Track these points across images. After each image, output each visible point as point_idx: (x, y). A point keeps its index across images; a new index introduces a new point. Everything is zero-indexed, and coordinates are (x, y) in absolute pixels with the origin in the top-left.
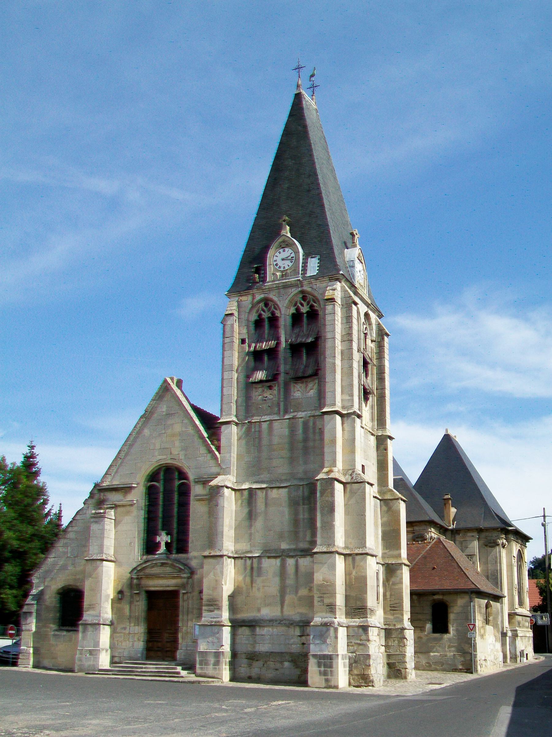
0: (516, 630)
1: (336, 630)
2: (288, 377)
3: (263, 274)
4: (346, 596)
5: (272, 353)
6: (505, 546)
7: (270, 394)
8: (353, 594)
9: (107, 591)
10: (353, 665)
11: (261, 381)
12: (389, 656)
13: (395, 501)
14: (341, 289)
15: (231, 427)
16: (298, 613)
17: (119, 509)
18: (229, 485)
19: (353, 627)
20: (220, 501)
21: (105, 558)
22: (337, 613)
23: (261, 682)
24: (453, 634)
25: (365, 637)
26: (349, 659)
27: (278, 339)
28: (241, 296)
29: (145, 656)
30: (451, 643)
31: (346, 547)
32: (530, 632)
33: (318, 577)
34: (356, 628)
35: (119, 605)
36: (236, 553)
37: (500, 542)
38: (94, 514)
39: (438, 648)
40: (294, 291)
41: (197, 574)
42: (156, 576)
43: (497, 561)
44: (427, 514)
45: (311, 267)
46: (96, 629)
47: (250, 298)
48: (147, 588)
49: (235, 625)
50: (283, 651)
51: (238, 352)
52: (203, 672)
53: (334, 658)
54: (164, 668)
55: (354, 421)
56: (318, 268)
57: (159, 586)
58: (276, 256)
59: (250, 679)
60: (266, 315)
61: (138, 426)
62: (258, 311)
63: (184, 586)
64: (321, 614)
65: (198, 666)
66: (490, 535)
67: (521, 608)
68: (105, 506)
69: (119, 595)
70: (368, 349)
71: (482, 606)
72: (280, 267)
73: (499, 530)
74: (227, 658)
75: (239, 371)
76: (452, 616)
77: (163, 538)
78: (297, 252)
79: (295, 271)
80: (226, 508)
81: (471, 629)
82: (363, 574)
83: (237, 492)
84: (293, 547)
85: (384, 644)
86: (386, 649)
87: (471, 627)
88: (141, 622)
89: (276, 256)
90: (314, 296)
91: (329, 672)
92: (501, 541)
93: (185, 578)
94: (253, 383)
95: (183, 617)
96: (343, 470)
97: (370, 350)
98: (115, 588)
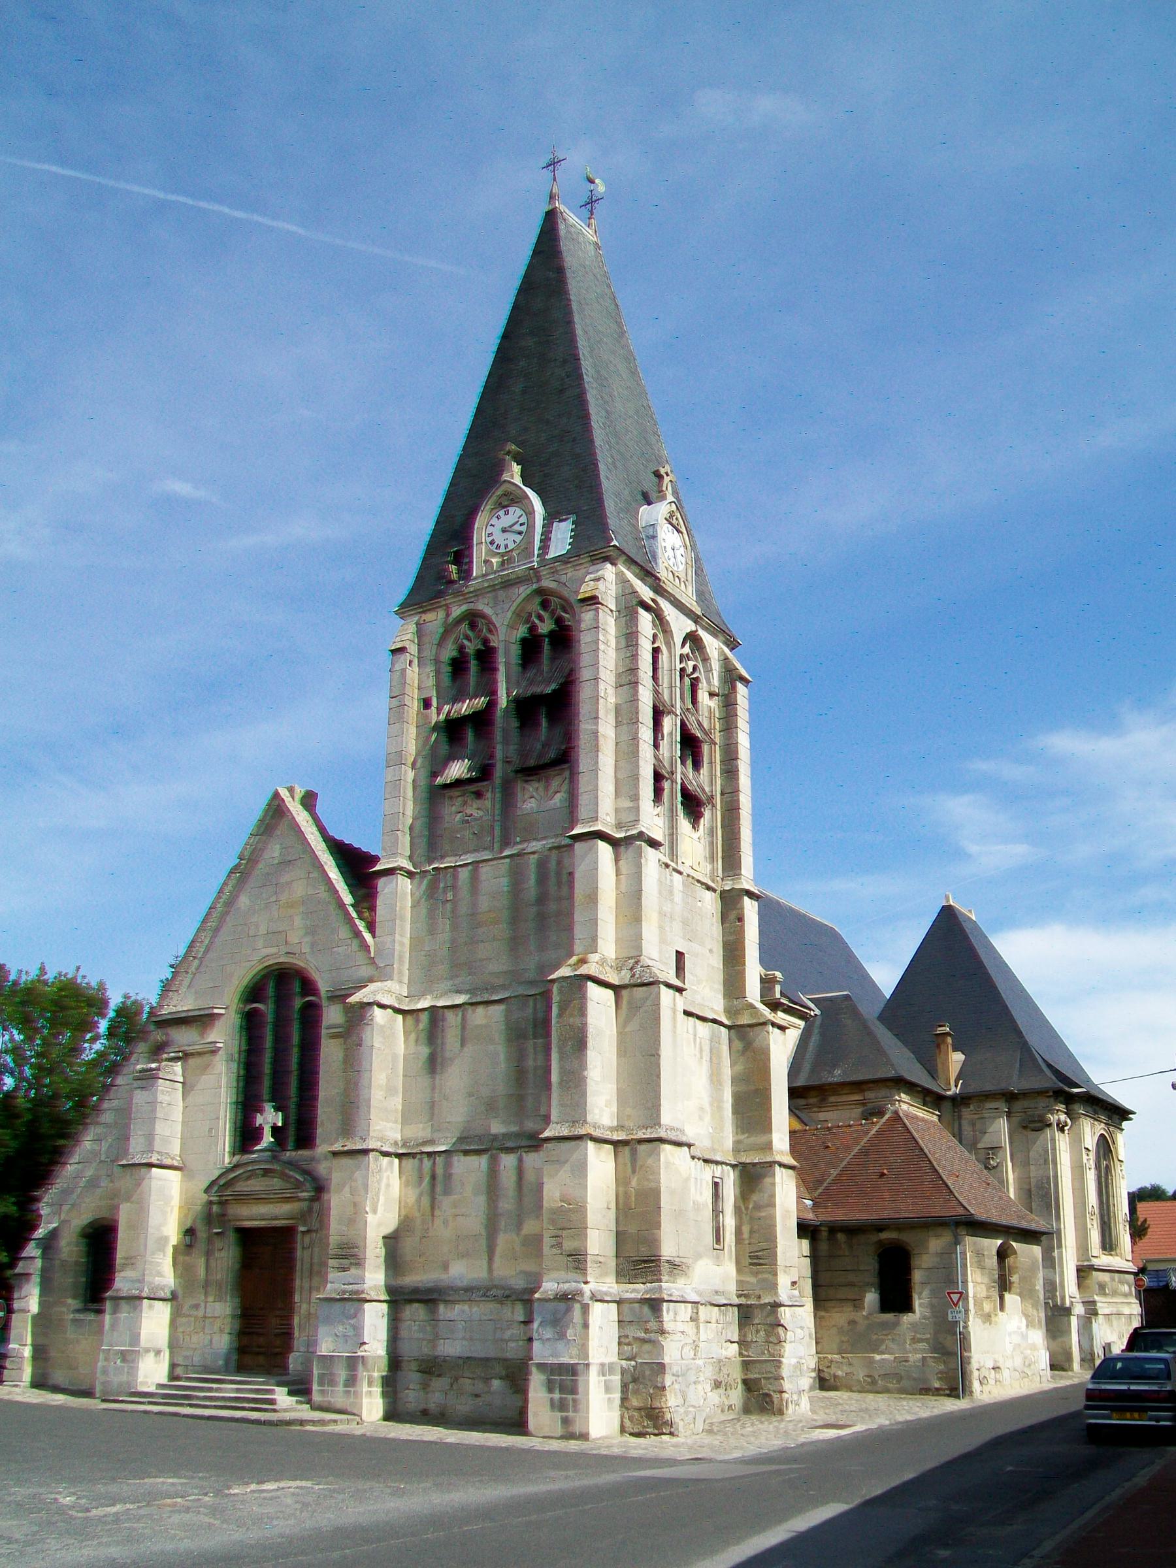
0: (1094, 1302)
1: (585, 1309)
2: (510, 768)
3: (466, 563)
4: (618, 1234)
5: (481, 720)
6: (1063, 1127)
7: (478, 809)
8: (632, 1229)
9: (162, 1228)
10: (630, 1387)
11: (458, 783)
12: (746, 1365)
13: (760, 1027)
14: (616, 578)
15: (395, 880)
16: (521, 1272)
17: (192, 1061)
18: (385, 1002)
19: (632, 1301)
20: (366, 1035)
21: (156, 1162)
22: (589, 1271)
23: (446, 1423)
24: (921, 1314)
25: (655, 1323)
26: (622, 1374)
27: (493, 693)
28: (424, 612)
29: (233, 1364)
30: (916, 1332)
31: (620, 1127)
32: (1134, 1306)
33: (552, 1193)
34: (637, 1305)
35: (187, 1258)
36: (404, 1145)
37: (1053, 1118)
38: (140, 1072)
39: (891, 1345)
40: (524, 591)
42: (252, 1197)
43: (1049, 1158)
44: (892, 1065)
45: (558, 539)
46: (135, 1308)
47: (441, 614)
48: (238, 1223)
49: (397, 1298)
50: (492, 1354)
51: (417, 727)
52: (326, 1399)
53: (580, 1372)
54: (251, 1391)
55: (640, 854)
56: (571, 540)
58: (492, 525)
59: (425, 1417)
60: (471, 647)
61: (227, 889)
62: (457, 640)
63: (304, 1216)
64: (554, 1275)
65: (315, 1387)
66: (1032, 1105)
67: (1111, 1255)
68: (165, 1056)
69: (186, 1237)
70: (702, 710)
71: (986, 1253)
72: (498, 547)
73: (1051, 1094)
74: (379, 1370)
75: (418, 765)
76: (917, 1276)
77: (269, 1118)
78: (530, 513)
79: (527, 550)
80: (379, 1049)
81: (954, 1303)
82: (653, 1185)
83: (409, 1018)
84: (514, 1129)
85: (736, 1338)
86: (740, 1348)
87: (955, 1297)
88: (226, 1293)
89: (492, 525)
90: (561, 598)
91: (571, 1402)
92: (1056, 1117)
93: (306, 1200)
94: (446, 786)
95: (302, 1283)
96: (616, 959)
97: (706, 714)
98: (180, 1224)
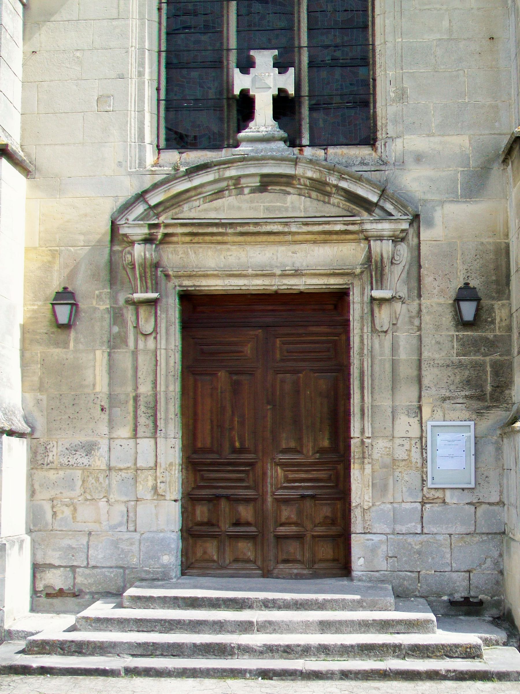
35: (56, 352)
41: (430, 224)
57: (250, 271)
